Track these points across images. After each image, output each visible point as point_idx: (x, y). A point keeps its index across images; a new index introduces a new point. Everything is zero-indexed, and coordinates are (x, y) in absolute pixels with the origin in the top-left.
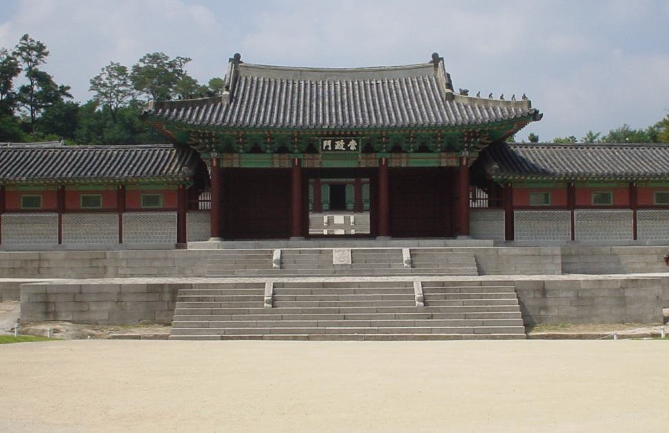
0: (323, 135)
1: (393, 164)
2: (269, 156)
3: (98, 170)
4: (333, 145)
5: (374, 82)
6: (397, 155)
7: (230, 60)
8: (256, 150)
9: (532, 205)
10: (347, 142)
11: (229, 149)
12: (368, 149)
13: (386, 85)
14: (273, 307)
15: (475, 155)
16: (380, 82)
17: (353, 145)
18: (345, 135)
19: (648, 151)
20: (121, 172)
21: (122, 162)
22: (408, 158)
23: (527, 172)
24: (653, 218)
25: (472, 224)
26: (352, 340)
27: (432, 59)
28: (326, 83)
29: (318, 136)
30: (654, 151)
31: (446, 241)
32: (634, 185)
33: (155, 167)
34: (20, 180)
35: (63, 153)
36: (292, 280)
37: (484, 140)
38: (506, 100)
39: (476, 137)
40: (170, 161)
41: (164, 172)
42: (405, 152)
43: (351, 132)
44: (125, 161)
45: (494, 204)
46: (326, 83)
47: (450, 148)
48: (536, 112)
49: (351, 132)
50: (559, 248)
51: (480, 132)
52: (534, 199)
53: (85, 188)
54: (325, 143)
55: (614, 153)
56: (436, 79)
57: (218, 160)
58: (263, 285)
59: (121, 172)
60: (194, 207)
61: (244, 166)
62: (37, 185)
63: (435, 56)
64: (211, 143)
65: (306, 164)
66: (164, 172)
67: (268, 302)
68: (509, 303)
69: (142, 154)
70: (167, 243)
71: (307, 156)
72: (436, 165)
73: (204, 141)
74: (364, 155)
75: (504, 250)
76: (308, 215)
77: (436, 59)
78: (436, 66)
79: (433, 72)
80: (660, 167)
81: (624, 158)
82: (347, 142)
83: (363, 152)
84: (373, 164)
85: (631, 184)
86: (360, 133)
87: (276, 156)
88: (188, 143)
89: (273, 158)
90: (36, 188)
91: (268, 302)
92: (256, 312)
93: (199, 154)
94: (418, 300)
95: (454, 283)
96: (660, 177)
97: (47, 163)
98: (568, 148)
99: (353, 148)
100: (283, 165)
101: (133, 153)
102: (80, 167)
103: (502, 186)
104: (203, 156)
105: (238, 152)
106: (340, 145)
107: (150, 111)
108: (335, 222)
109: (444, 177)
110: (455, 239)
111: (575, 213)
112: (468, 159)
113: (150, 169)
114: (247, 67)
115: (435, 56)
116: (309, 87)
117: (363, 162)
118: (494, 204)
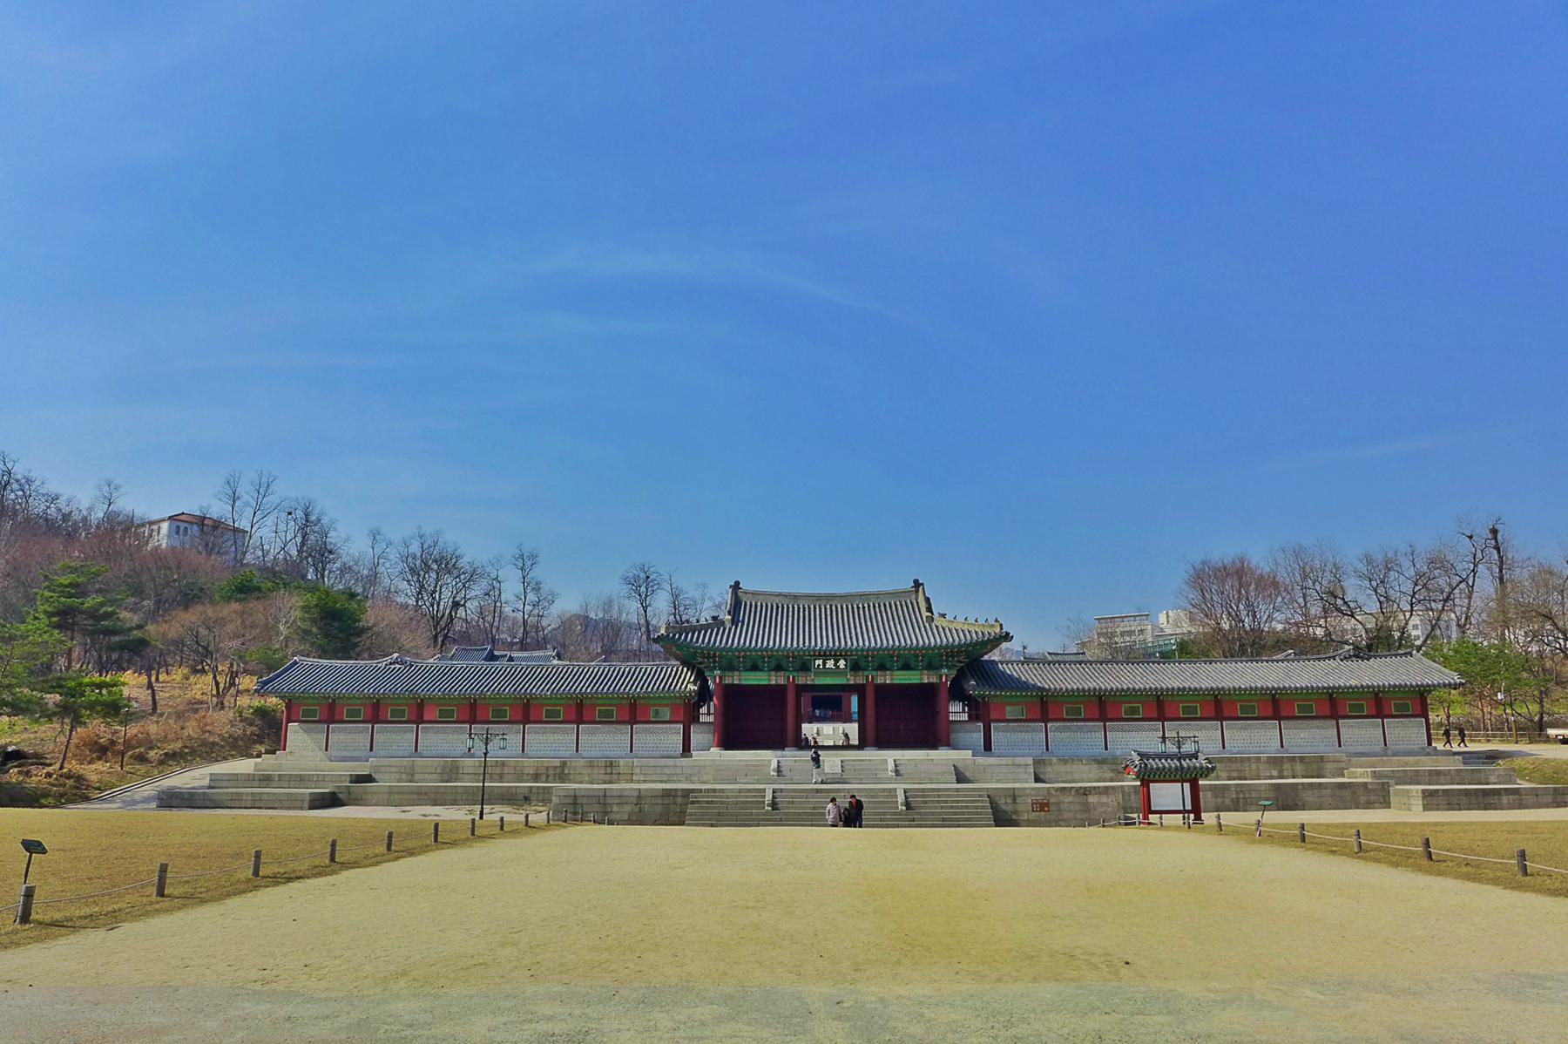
0: (814, 655)
1: (879, 681)
2: (766, 674)
3: (613, 685)
4: (824, 664)
5: (860, 606)
6: (883, 673)
7: (731, 587)
8: (755, 668)
9: (1009, 718)
10: (836, 661)
11: (730, 667)
12: (855, 667)
13: (872, 608)
14: (773, 810)
15: (954, 672)
16: (866, 605)
17: (842, 663)
18: (835, 655)
19: (1206, 666)
20: (634, 688)
21: (634, 678)
22: (892, 675)
23: (1001, 687)
24: (1317, 728)
25: (952, 736)
26: (1046, 826)
27: (913, 584)
28: (817, 607)
29: (811, 656)
30: (1122, 667)
31: (929, 751)
32: (1334, 696)
33: (663, 683)
34: (419, 694)
35: (581, 670)
36: (789, 787)
37: (961, 659)
38: (981, 623)
39: (953, 657)
40: (677, 677)
41: (672, 687)
42: (889, 670)
43: (841, 653)
44: (544, 675)
45: (973, 718)
46: (817, 607)
47: (931, 666)
48: (1008, 634)
49: (841, 653)
50: (1031, 758)
51: (957, 652)
52: (1010, 712)
53: (601, 702)
54: (817, 662)
55: (1084, 669)
56: (917, 603)
57: (720, 678)
58: (764, 790)
59: (634, 688)
60: (696, 720)
61: (744, 683)
62: (559, 699)
63: (916, 582)
64: (715, 662)
65: (800, 681)
66: (672, 687)
67: (768, 805)
68: (982, 807)
69: (651, 670)
70: (673, 752)
71: (727, 673)
72: (918, 682)
73: (708, 660)
74: (852, 673)
75: (981, 760)
76: (10, 752)
77: (917, 584)
78: (917, 591)
79: (914, 596)
80: (1126, 682)
81: (1093, 673)
82: (836, 661)
83: (851, 670)
84: (860, 680)
85: (1100, 698)
86: (843, 653)
87: (773, 673)
88: (695, 661)
89: (769, 676)
90: (557, 702)
91: (768, 805)
92: (758, 814)
93: (704, 672)
94: (902, 805)
95: (933, 790)
96: (1126, 692)
97: (568, 678)
98: (1041, 665)
99: (842, 666)
100: (779, 682)
101: (643, 670)
102: (596, 683)
103: (980, 700)
104: (707, 674)
105: (738, 670)
106: (830, 664)
107: (662, 634)
108: (825, 733)
109: (928, 691)
110: (937, 750)
111: (1049, 725)
112: (946, 676)
113: (659, 685)
114: (746, 593)
115: (916, 582)
116: (801, 610)
117: (851, 680)
118: (973, 718)
